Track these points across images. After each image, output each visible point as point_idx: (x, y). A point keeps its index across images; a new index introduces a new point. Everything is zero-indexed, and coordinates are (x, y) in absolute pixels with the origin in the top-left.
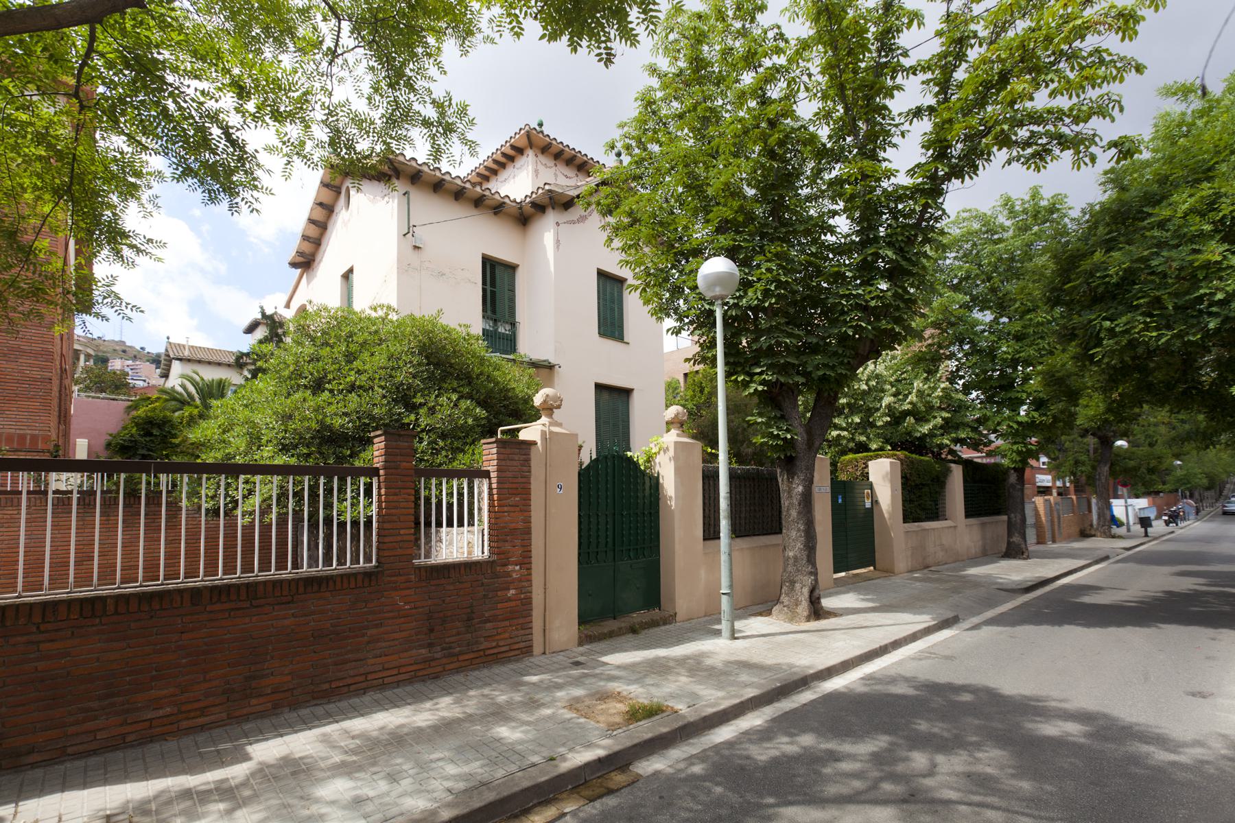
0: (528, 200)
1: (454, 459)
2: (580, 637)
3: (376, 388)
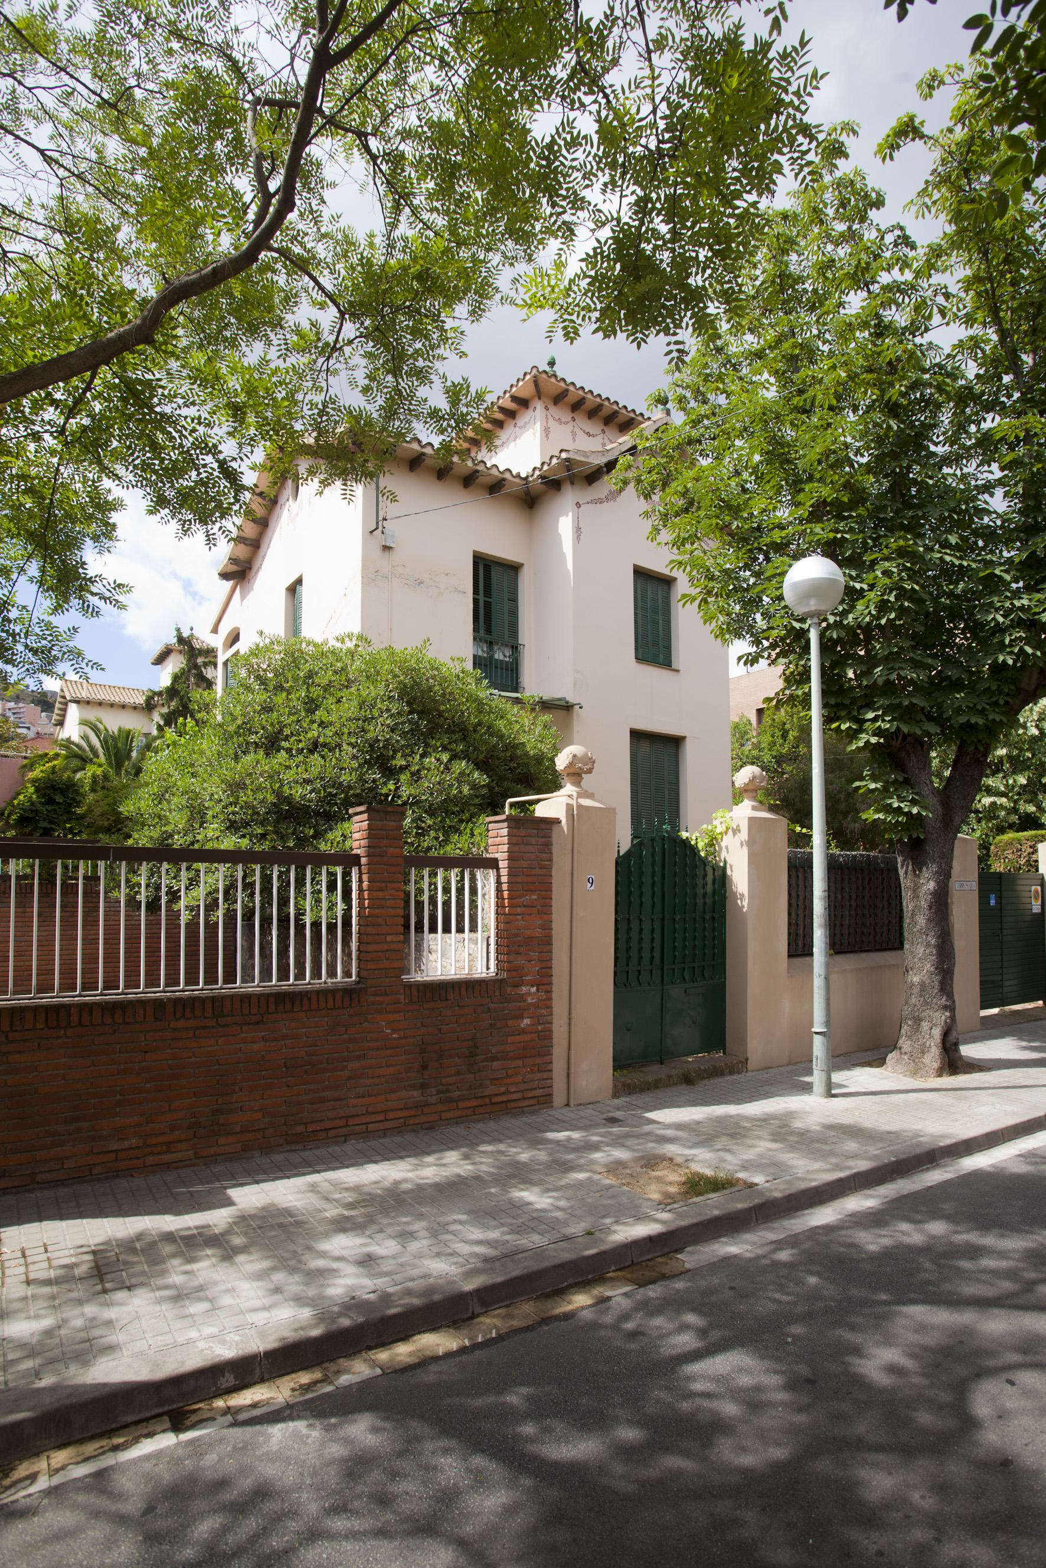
0: (537, 473)
1: (446, 841)
2: (615, 1086)
3: (345, 747)
